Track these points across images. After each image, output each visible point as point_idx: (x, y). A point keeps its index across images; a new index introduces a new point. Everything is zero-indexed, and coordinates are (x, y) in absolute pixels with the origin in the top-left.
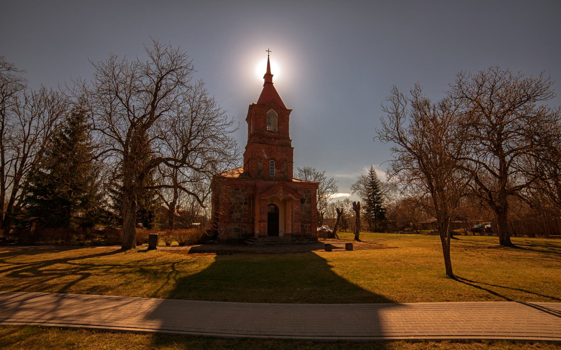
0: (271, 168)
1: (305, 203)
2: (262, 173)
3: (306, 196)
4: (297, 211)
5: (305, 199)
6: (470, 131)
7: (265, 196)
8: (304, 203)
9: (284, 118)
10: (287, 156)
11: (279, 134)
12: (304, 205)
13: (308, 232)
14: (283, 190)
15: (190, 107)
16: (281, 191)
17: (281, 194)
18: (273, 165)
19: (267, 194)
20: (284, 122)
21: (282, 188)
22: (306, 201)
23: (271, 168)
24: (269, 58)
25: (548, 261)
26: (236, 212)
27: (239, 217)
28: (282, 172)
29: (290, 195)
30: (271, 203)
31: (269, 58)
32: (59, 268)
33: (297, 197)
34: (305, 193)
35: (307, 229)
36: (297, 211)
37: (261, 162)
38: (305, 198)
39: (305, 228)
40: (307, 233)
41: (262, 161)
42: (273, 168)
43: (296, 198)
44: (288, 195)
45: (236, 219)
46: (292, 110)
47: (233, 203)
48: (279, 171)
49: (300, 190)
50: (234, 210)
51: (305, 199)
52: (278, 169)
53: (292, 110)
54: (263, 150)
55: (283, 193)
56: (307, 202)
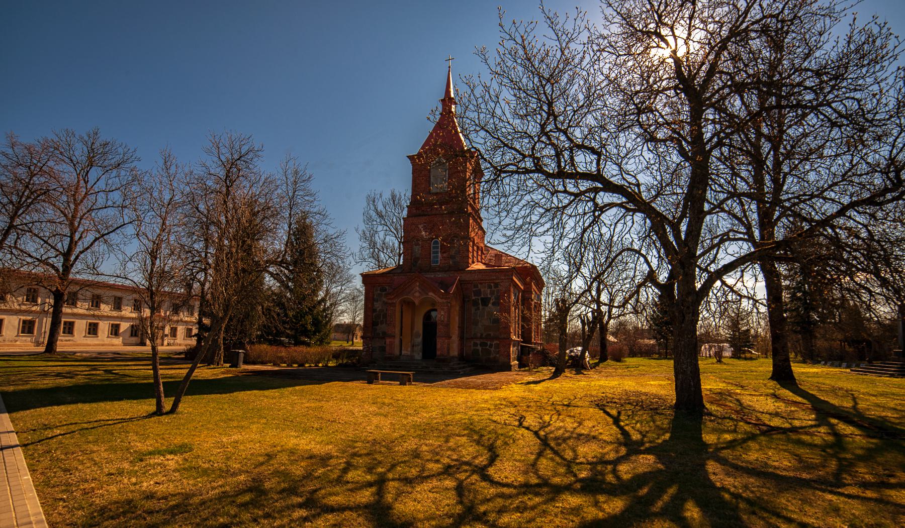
0: (434, 253)
1: (490, 305)
2: (419, 262)
3: (492, 293)
6: (558, 155)
8: (487, 306)
15: (23, 247)
16: (417, 288)
17: (417, 294)
18: (437, 248)
22: (492, 301)
23: (434, 253)
25: (110, 425)
28: (452, 257)
29: (431, 294)
30: (431, 308)
32: (799, 399)
34: (490, 287)
35: (493, 349)
37: (417, 244)
38: (489, 296)
40: (492, 356)
41: (420, 243)
42: (437, 252)
43: (442, 298)
44: (427, 294)
48: (444, 255)
49: (481, 283)
52: (444, 252)
54: (420, 227)
56: (494, 304)
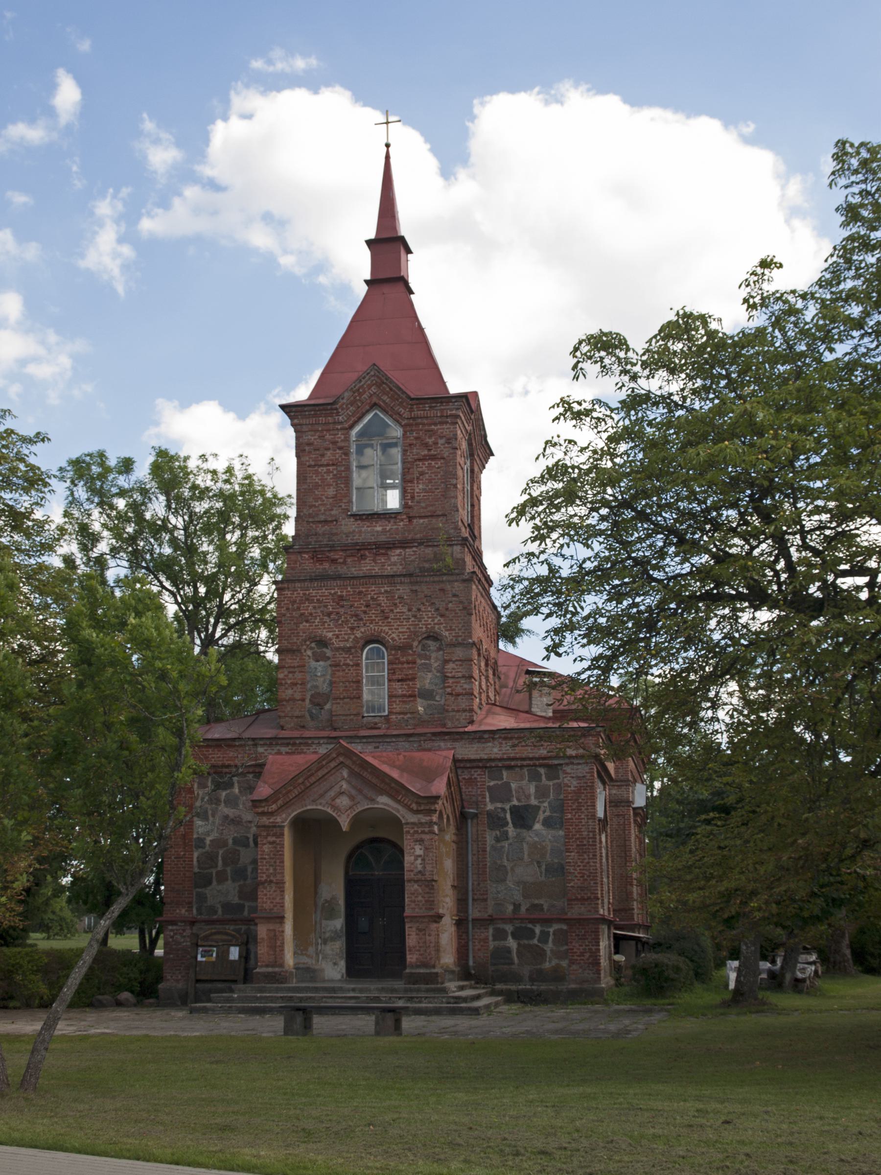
1: (537, 826)
3: (542, 793)
4: (420, 867)
5: (538, 808)
7: (271, 814)
8: (529, 827)
9: (430, 441)
10: (442, 616)
11: (410, 519)
12: (530, 837)
13: (554, 962)
14: (349, 782)
16: (345, 785)
17: (343, 801)
19: (280, 802)
20: (433, 458)
21: (345, 773)
22: (541, 816)
24: (388, 157)
26: (222, 878)
27: (236, 900)
31: (388, 157)
33: (414, 806)
35: (549, 946)
36: (420, 867)
38: (534, 802)
39: (535, 941)
45: (222, 907)
46: (283, 407)
47: (208, 842)
50: (214, 871)
51: (538, 808)
53: (283, 407)
55: (352, 798)
56: (547, 823)
